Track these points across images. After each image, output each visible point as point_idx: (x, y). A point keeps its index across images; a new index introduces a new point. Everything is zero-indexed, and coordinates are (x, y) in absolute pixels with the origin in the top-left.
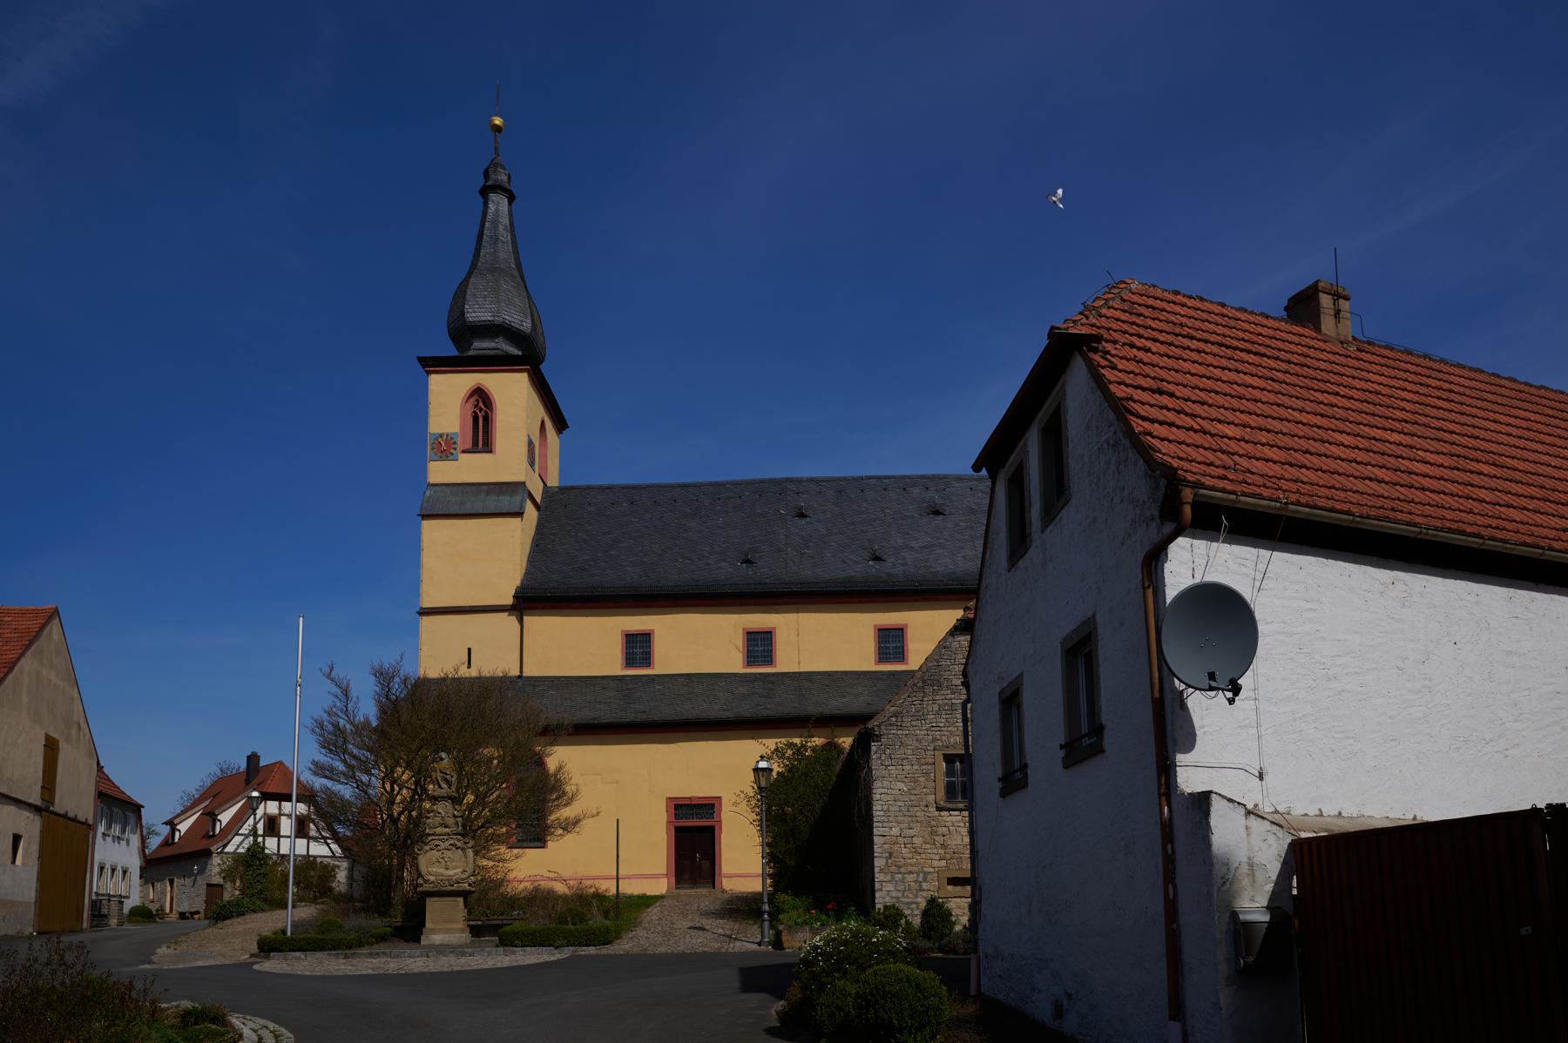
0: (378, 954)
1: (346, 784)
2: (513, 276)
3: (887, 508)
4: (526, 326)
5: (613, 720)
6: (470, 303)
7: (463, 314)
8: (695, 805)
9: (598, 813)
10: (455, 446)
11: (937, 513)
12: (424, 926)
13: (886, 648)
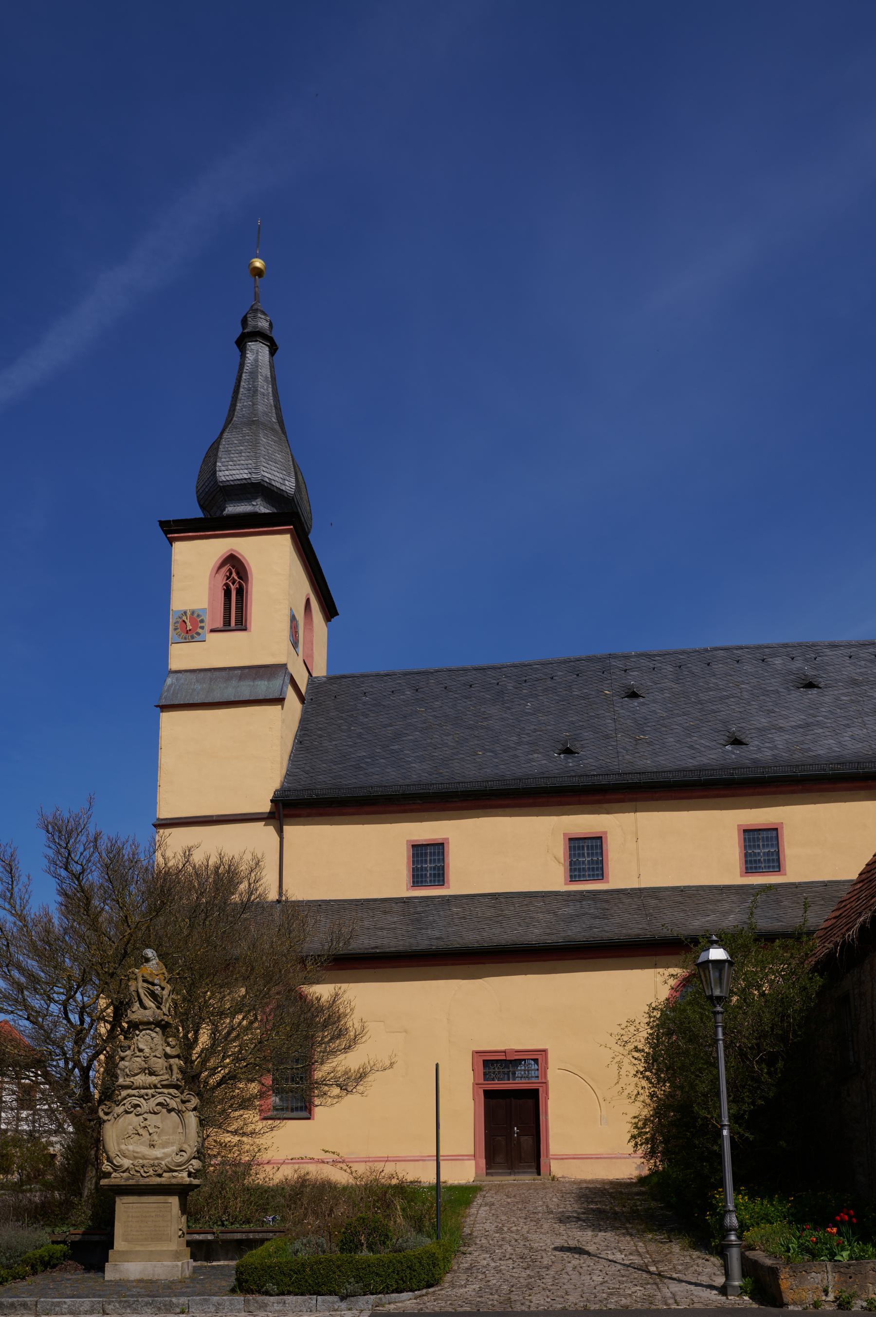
0: (12, 1305)
1: (12, 1012)
2: (273, 430)
3: (743, 683)
4: (289, 485)
5: (401, 948)
6: (223, 460)
7: (214, 473)
8: (511, 1061)
9: (392, 1065)
10: (202, 625)
11: (810, 685)
12: (111, 1245)
13: (755, 854)
